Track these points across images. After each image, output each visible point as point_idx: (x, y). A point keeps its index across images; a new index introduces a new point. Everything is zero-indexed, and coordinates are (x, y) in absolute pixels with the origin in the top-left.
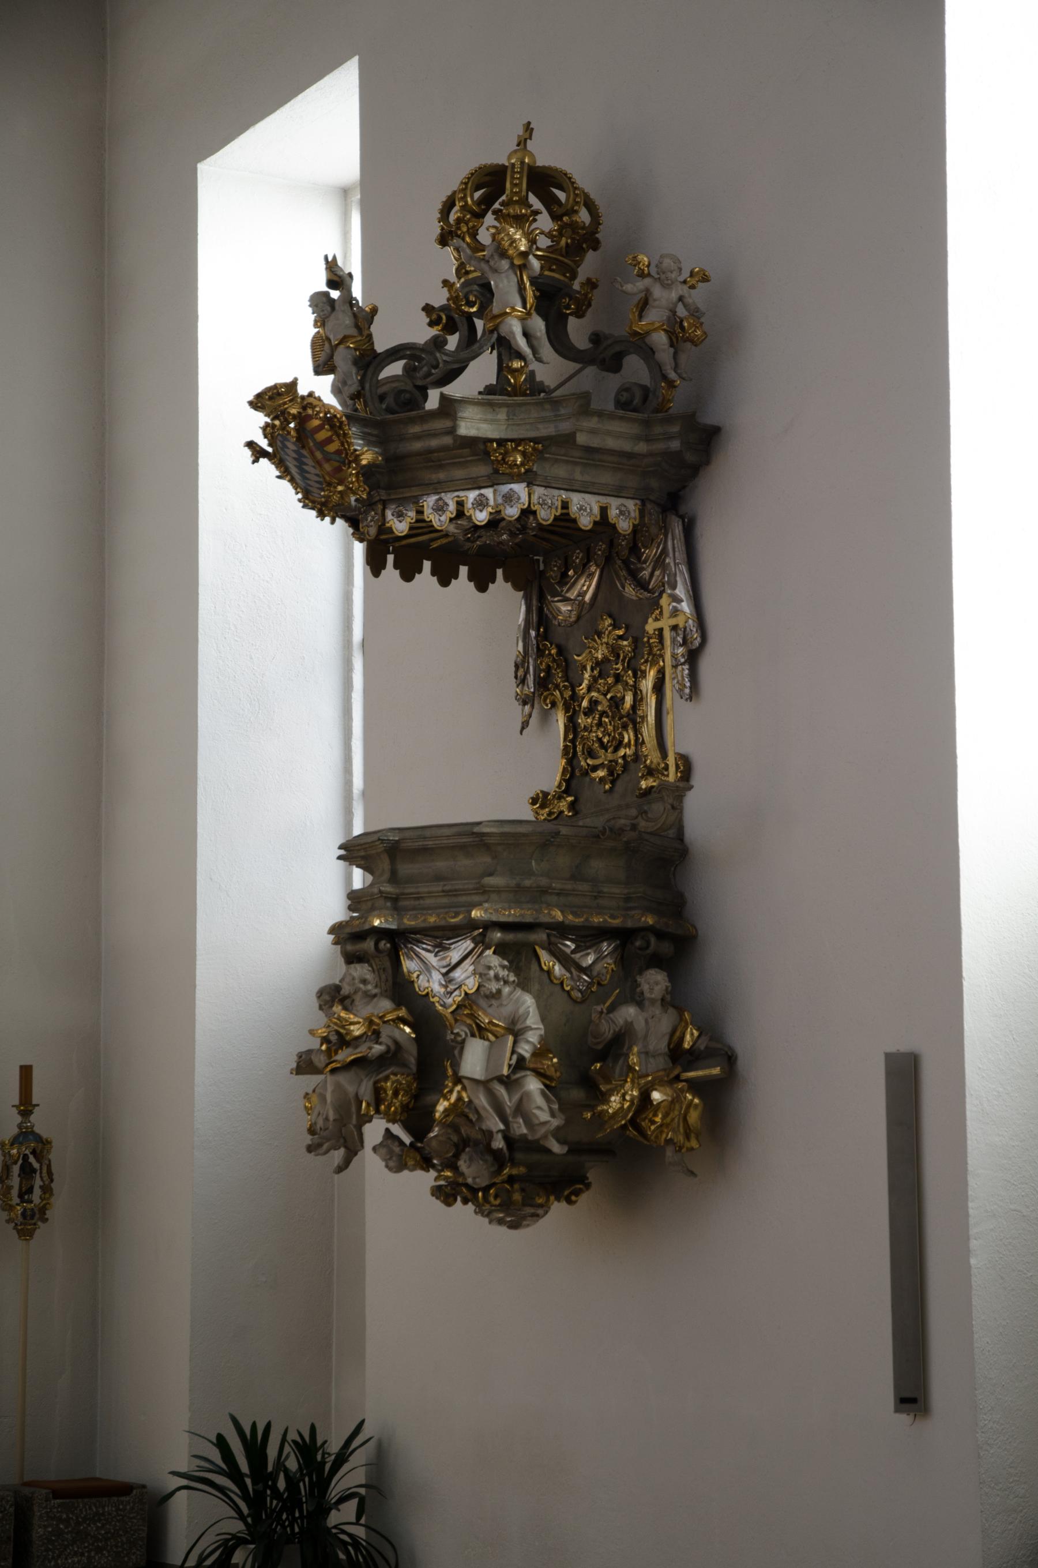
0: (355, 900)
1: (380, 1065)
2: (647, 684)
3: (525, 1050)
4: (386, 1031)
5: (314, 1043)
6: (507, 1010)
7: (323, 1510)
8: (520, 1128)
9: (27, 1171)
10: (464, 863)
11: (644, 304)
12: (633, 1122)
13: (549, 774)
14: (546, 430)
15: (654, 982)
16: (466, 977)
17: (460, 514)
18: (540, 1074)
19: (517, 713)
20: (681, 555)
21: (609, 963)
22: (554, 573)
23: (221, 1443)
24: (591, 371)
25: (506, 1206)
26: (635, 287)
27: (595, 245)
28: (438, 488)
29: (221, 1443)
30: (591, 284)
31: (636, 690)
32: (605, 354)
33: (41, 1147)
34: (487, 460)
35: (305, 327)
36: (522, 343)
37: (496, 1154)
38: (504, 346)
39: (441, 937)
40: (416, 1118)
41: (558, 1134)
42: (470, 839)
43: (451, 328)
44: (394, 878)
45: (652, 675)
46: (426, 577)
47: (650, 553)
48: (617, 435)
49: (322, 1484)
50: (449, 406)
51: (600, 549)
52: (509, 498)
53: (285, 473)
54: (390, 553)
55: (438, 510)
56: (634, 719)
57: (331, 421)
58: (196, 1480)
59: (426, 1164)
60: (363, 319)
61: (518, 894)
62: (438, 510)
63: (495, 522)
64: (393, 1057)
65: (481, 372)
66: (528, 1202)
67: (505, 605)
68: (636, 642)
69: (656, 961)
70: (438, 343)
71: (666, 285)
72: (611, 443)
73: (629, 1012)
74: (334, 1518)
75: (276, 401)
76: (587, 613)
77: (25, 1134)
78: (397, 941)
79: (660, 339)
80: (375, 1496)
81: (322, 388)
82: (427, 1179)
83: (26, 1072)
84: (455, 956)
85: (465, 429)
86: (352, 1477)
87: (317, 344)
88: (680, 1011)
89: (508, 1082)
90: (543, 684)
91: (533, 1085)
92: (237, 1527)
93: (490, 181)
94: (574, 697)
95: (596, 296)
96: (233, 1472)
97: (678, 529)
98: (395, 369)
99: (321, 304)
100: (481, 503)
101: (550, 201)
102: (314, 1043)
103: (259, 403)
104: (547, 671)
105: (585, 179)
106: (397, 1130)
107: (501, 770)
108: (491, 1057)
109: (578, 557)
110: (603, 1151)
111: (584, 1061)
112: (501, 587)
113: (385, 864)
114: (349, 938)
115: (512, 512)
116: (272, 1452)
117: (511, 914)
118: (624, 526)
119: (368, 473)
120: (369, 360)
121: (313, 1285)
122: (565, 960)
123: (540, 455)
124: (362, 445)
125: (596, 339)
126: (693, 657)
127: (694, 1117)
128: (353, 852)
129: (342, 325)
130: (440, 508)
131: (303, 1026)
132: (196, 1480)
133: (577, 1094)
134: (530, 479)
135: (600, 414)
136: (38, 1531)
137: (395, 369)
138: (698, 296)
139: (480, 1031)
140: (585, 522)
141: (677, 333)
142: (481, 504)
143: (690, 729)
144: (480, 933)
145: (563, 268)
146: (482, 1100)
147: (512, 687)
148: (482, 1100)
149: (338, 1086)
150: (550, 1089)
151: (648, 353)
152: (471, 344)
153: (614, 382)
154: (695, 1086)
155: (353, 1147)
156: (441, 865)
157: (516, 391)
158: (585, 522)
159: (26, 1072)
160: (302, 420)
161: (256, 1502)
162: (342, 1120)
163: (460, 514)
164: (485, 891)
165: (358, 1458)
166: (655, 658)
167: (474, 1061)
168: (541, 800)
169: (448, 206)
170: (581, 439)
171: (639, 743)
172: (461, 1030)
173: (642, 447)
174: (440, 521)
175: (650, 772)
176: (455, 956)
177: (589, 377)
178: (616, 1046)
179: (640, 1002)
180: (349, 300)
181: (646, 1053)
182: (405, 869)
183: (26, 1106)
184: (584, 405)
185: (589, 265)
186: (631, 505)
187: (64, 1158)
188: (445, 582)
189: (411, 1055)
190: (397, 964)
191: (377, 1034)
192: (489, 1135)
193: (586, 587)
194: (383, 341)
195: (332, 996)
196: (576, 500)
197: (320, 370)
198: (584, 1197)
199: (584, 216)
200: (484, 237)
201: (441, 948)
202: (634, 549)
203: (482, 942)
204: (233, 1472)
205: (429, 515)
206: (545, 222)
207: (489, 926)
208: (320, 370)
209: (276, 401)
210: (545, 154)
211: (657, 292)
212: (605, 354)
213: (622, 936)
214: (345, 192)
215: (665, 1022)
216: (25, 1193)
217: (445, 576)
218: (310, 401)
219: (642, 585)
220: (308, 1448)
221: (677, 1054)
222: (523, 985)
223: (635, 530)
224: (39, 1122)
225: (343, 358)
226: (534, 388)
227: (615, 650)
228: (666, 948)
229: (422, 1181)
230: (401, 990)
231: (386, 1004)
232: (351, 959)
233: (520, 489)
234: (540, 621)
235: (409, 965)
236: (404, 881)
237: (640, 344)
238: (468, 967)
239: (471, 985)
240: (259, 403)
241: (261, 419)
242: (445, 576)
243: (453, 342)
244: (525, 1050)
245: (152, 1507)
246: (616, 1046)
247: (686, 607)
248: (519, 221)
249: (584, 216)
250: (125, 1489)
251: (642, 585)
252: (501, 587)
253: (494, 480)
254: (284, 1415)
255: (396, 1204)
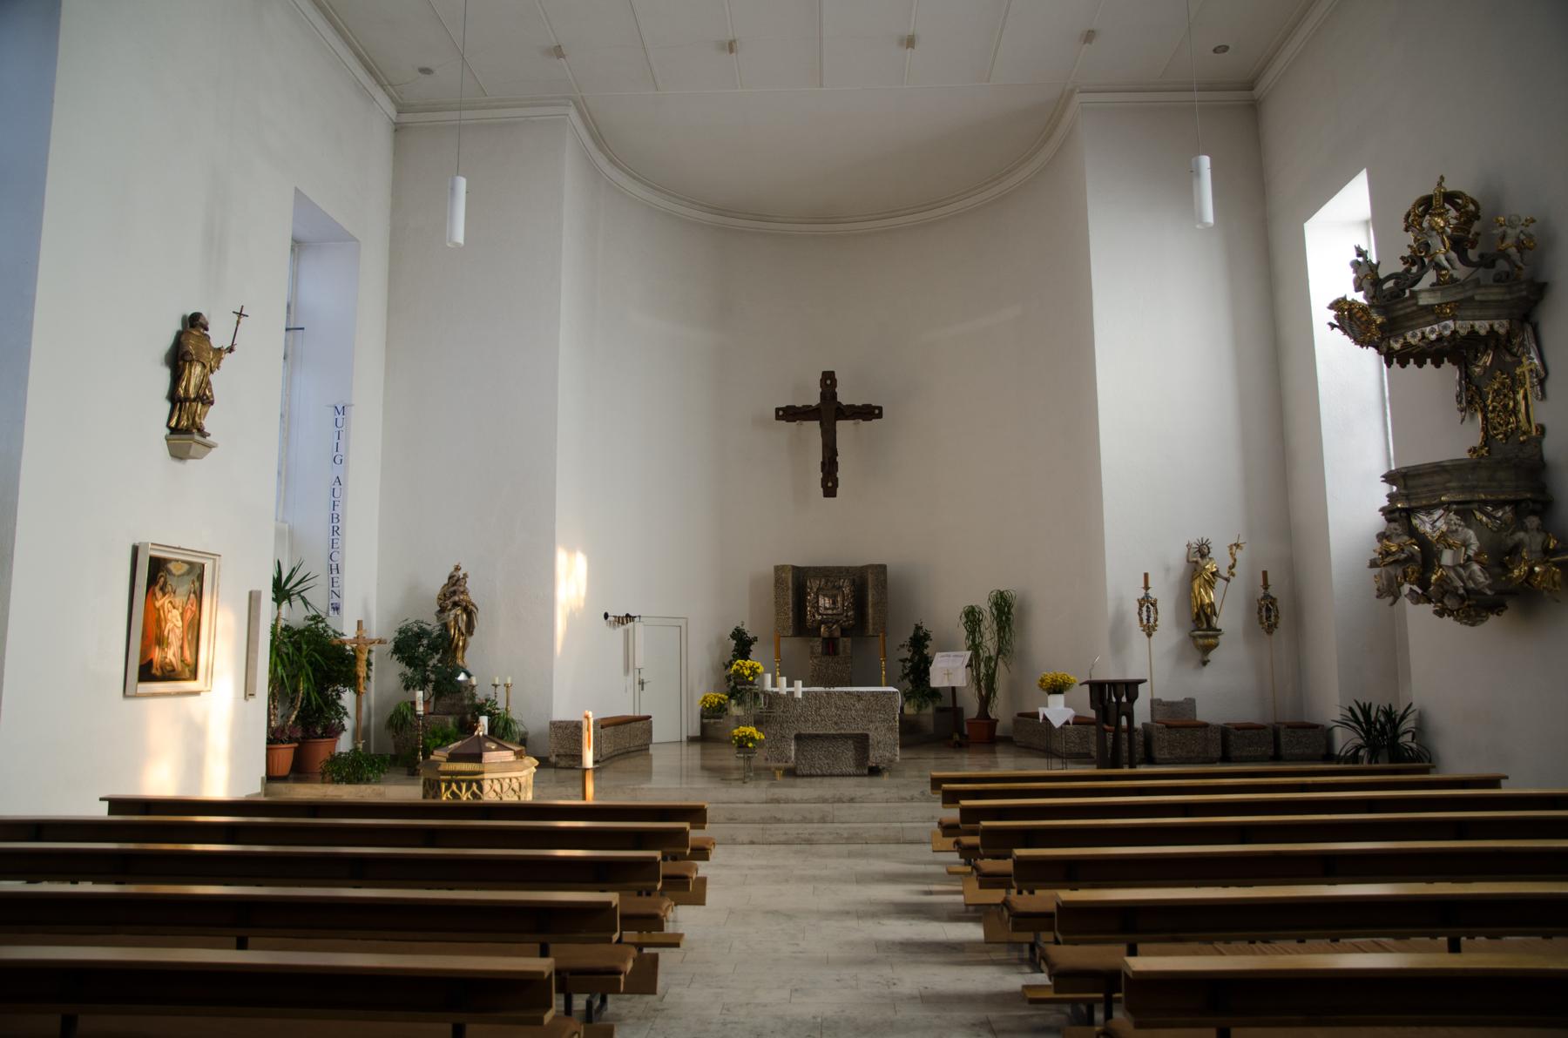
0: (1391, 497)
1: (1406, 562)
2: (1520, 396)
3: (1471, 553)
4: (1406, 549)
5: (1376, 555)
6: (1461, 537)
7: (1397, 736)
8: (1471, 585)
9: (1268, 610)
10: (1437, 479)
11: (1503, 237)
12: (1527, 580)
13: (1476, 439)
14: (1459, 297)
15: (1532, 521)
16: (1441, 525)
17: (1424, 337)
18: (1478, 562)
19: (1459, 416)
20: (1532, 340)
21: (1510, 515)
22: (1471, 355)
23: (1351, 710)
24: (1481, 270)
25: (1468, 617)
26: (1498, 231)
27: (1478, 218)
28: (1412, 328)
29: (1351, 710)
30: (1477, 234)
31: (1515, 400)
32: (1487, 261)
33: (1273, 601)
34: (1434, 313)
35: (1350, 275)
36: (1445, 263)
37: (1461, 596)
38: (1438, 267)
39: (1429, 510)
40: (1423, 583)
41: (1489, 587)
42: (1438, 469)
43: (1413, 264)
44: (1406, 487)
45: (1522, 392)
46: (1412, 365)
47: (1516, 341)
48: (1495, 294)
49: (1395, 726)
50: (1414, 295)
51: (1492, 343)
52: (1445, 327)
53: (1345, 332)
54: (1389, 357)
55: (1413, 337)
56: (1515, 412)
57: (1363, 309)
58: (1344, 724)
59: (1429, 601)
60: (1373, 268)
61: (1463, 489)
62: (1413, 337)
63: (1440, 338)
64: (1411, 558)
65: (1430, 277)
66: (1478, 615)
67: (1449, 373)
68: (1513, 380)
69: (1534, 513)
70: (1408, 271)
71: (1513, 227)
72: (1492, 297)
73: (1521, 535)
74: (1401, 740)
75: (1339, 305)
76: (1489, 372)
77: (1266, 596)
78: (1409, 513)
79: (1513, 250)
80: (1419, 731)
81: (1360, 297)
82: (1430, 608)
83: (1265, 573)
84: (1436, 516)
85: (1421, 302)
86: (1408, 724)
87: (1355, 281)
88: (1547, 533)
89: (1464, 566)
90: (1470, 403)
91: (1476, 567)
92: (1361, 741)
93: (1426, 203)
94: (1486, 406)
95: (1480, 239)
96: (1357, 720)
97: (1529, 329)
98: (1390, 284)
99: (1356, 265)
100: (1432, 331)
101: (1454, 205)
102: (1376, 555)
103: (1331, 307)
104: (1471, 397)
105: (1468, 192)
106: (1415, 588)
107: (1455, 439)
108: (1455, 556)
109: (1482, 348)
110: (1512, 593)
111: (1500, 556)
112: (1447, 365)
113: (1401, 482)
114: (1388, 512)
115: (1447, 333)
116: (1373, 713)
117: (1460, 498)
118: (1502, 331)
119: (1381, 327)
120: (1377, 283)
121: (1390, 650)
122: (1488, 515)
123: (1458, 308)
124: (1379, 317)
125: (1481, 256)
126: (1542, 382)
127: (1557, 577)
128: (1389, 478)
129: (1366, 273)
130: (1414, 336)
131: (1371, 548)
132: (1344, 724)
133: (1498, 570)
134: (1454, 318)
135: (1486, 286)
136: (1283, 740)
137: (1390, 284)
138: (1531, 229)
139: (1450, 546)
140: (1483, 332)
141: (1520, 246)
142: (1432, 332)
143: (1541, 413)
144: (1446, 506)
145: (1463, 230)
146: (1452, 574)
147: (1456, 405)
148: (1452, 574)
149: (1388, 573)
150: (1484, 567)
151: (1507, 257)
152: (1423, 269)
153: (1493, 272)
154: (1556, 564)
155: (1396, 596)
156: (1427, 480)
157: (1445, 283)
158: (1483, 332)
159: (1265, 573)
160: (1350, 310)
161: (1368, 733)
162: (1390, 584)
163: (1424, 337)
164: (1447, 490)
165: (1411, 717)
166: (1523, 385)
167: (1447, 558)
168: (1473, 450)
169: (1408, 215)
170: (1477, 298)
171: (1518, 421)
172: (1440, 546)
173: (1508, 297)
174: (1413, 341)
175: (1524, 433)
176: (1436, 516)
177: (1481, 272)
178: (1515, 550)
179: (1526, 530)
180: (1368, 262)
181: (1530, 552)
182: (1410, 483)
183: (1266, 586)
184: (1477, 284)
185: (1476, 227)
186: (1505, 322)
187: (1283, 605)
188: (1420, 366)
189: (1419, 558)
190: (1410, 522)
191: (1402, 551)
192: (1456, 588)
193: (1488, 359)
194: (1382, 274)
195: (1382, 536)
196: (1477, 324)
197: (1358, 289)
198: (1505, 614)
199: (1472, 207)
200: (1425, 224)
201: (1429, 514)
202: (1509, 340)
203: (1447, 510)
204: (1357, 720)
205: (1409, 339)
206: (1453, 213)
207: (1450, 503)
208: (1358, 289)
209: (1339, 305)
210: (1449, 186)
211: (1509, 231)
212: (1487, 261)
213: (1515, 504)
214: (1367, 222)
215: (1539, 538)
216: (1268, 618)
217: (1420, 364)
218: (1353, 303)
219: (1514, 355)
220: (1388, 714)
221: (1546, 551)
222: (1469, 526)
223: (1508, 332)
224: (1272, 592)
225: (1366, 284)
226: (1453, 280)
227: (1503, 384)
228: (1538, 507)
229: (1428, 609)
230: (1413, 532)
231: (1406, 538)
232: (1389, 521)
233: (1450, 323)
234: (1467, 377)
235: (1415, 522)
236: (1410, 488)
237: (1504, 254)
238: (1442, 520)
239: (1444, 528)
240: (1331, 307)
241: (1333, 313)
242: (1420, 364)
243: (1414, 269)
244: (1471, 553)
245: (1327, 734)
246: (1515, 550)
247: (1536, 361)
248: (1440, 215)
249: (1472, 207)
250: (1315, 727)
251: (1514, 355)
252: (1447, 365)
253: (1437, 322)
254: (1378, 701)
255: (1419, 618)
